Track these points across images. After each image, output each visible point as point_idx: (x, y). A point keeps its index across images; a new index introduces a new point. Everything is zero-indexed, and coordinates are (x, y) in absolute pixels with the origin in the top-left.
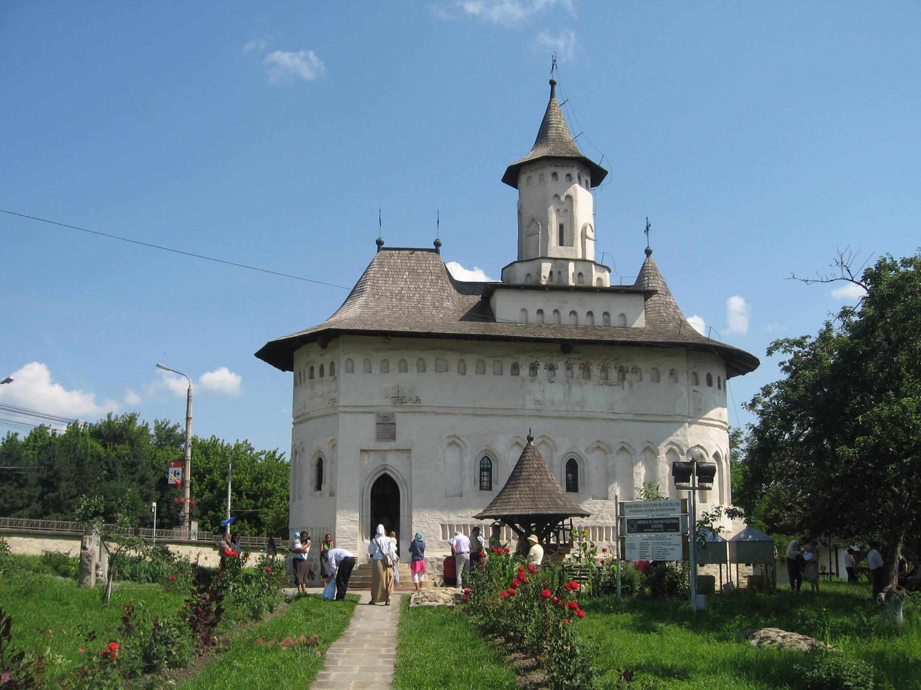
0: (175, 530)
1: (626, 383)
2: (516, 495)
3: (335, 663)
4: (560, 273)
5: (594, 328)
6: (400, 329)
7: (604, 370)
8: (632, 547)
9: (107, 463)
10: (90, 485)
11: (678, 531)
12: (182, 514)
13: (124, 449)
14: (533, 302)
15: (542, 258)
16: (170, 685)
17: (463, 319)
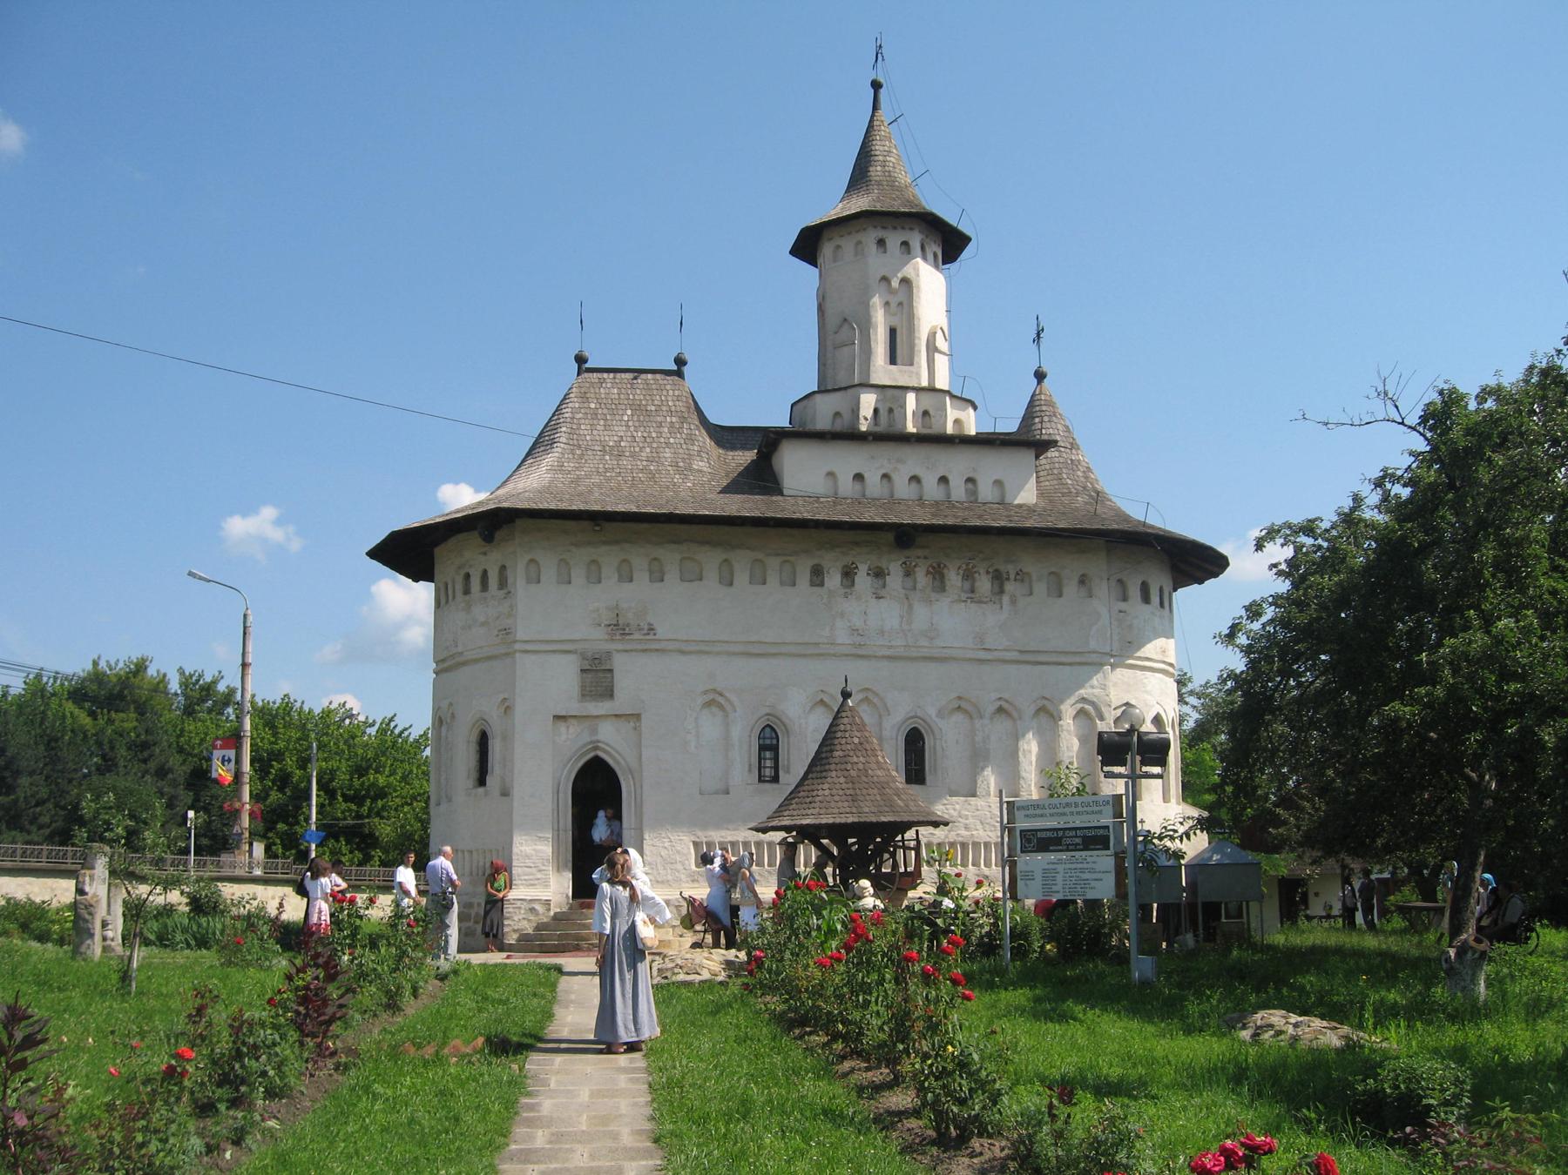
0: (225, 858)
1: (1006, 599)
2: (824, 790)
3: (545, 1083)
4: (891, 411)
5: (950, 504)
6: (621, 508)
7: (968, 576)
8: (1029, 876)
9: (99, 744)
10: (70, 781)
11: (1108, 848)
12: (236, 829)
13: (127, 721)
14: (846, 461)
15: (860, 385)
16: (270, 1129)
17: (725, 490)
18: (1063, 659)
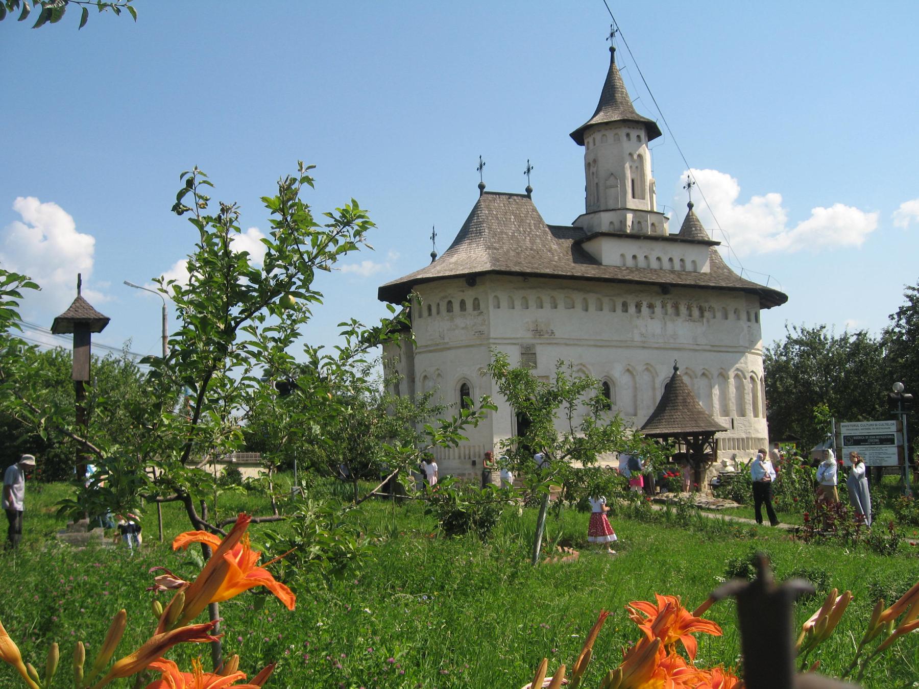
1: (705, 320)
7: (689, 308)
14: (630, 249)
18: (730, 350)
